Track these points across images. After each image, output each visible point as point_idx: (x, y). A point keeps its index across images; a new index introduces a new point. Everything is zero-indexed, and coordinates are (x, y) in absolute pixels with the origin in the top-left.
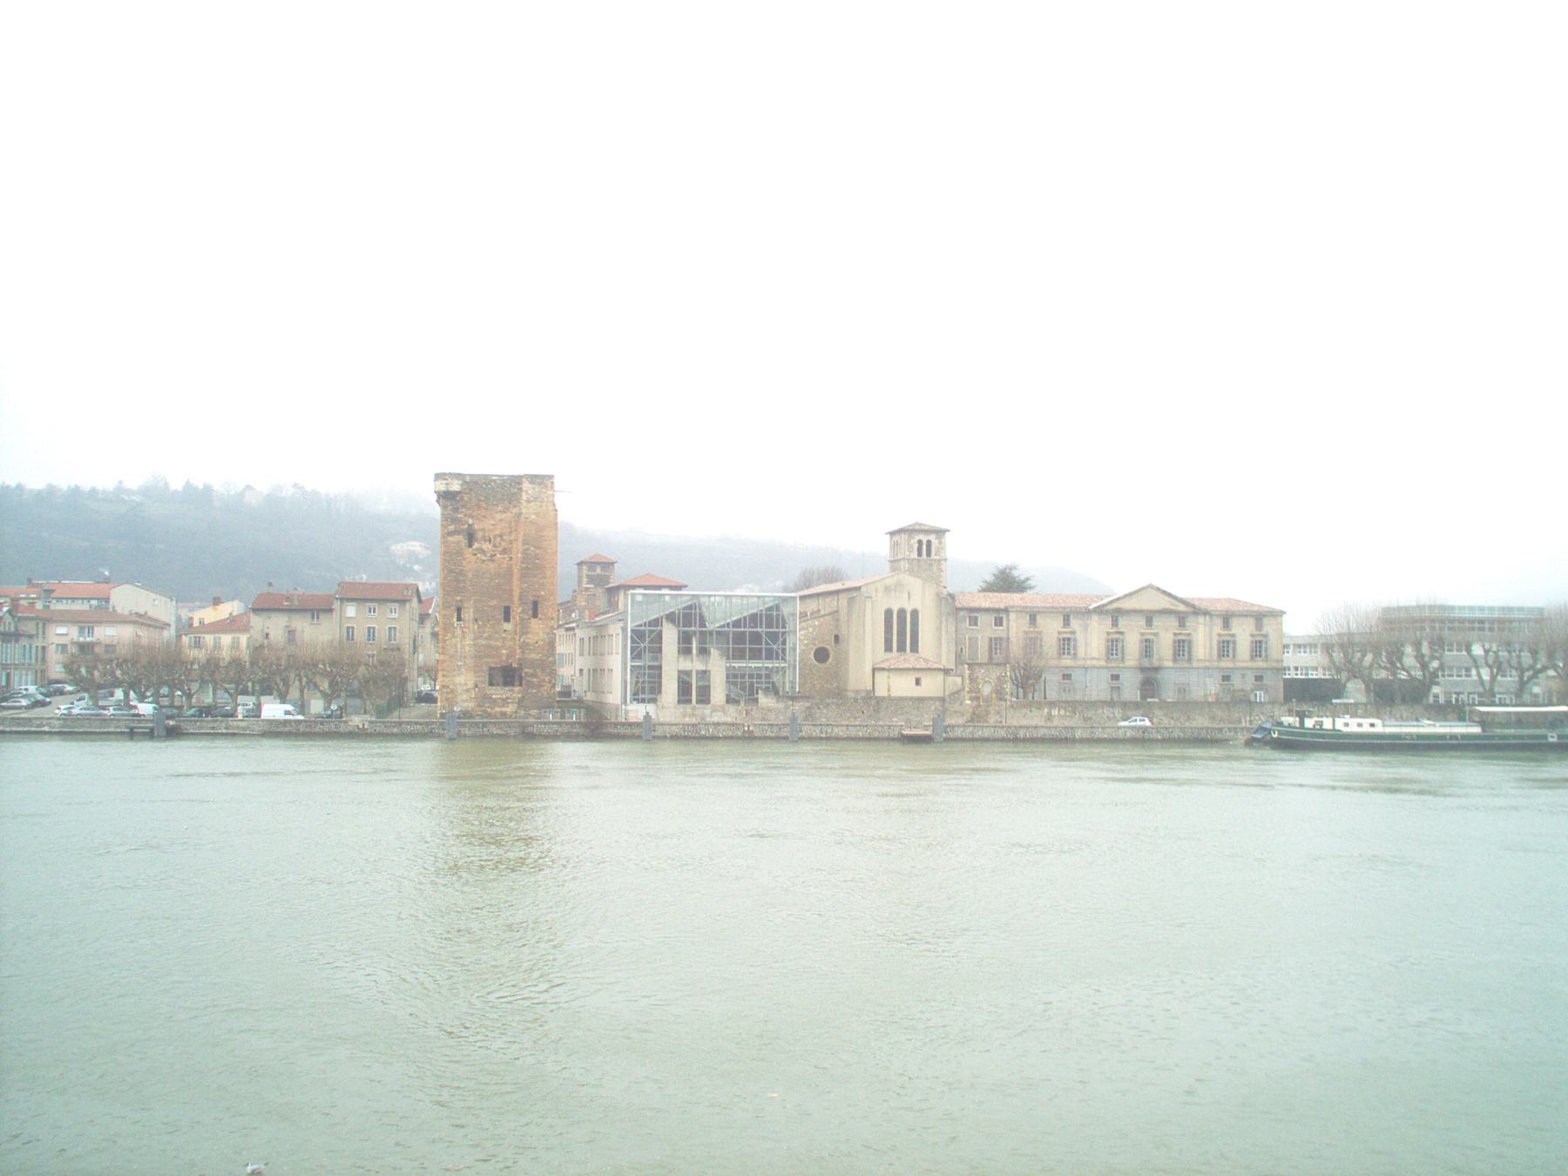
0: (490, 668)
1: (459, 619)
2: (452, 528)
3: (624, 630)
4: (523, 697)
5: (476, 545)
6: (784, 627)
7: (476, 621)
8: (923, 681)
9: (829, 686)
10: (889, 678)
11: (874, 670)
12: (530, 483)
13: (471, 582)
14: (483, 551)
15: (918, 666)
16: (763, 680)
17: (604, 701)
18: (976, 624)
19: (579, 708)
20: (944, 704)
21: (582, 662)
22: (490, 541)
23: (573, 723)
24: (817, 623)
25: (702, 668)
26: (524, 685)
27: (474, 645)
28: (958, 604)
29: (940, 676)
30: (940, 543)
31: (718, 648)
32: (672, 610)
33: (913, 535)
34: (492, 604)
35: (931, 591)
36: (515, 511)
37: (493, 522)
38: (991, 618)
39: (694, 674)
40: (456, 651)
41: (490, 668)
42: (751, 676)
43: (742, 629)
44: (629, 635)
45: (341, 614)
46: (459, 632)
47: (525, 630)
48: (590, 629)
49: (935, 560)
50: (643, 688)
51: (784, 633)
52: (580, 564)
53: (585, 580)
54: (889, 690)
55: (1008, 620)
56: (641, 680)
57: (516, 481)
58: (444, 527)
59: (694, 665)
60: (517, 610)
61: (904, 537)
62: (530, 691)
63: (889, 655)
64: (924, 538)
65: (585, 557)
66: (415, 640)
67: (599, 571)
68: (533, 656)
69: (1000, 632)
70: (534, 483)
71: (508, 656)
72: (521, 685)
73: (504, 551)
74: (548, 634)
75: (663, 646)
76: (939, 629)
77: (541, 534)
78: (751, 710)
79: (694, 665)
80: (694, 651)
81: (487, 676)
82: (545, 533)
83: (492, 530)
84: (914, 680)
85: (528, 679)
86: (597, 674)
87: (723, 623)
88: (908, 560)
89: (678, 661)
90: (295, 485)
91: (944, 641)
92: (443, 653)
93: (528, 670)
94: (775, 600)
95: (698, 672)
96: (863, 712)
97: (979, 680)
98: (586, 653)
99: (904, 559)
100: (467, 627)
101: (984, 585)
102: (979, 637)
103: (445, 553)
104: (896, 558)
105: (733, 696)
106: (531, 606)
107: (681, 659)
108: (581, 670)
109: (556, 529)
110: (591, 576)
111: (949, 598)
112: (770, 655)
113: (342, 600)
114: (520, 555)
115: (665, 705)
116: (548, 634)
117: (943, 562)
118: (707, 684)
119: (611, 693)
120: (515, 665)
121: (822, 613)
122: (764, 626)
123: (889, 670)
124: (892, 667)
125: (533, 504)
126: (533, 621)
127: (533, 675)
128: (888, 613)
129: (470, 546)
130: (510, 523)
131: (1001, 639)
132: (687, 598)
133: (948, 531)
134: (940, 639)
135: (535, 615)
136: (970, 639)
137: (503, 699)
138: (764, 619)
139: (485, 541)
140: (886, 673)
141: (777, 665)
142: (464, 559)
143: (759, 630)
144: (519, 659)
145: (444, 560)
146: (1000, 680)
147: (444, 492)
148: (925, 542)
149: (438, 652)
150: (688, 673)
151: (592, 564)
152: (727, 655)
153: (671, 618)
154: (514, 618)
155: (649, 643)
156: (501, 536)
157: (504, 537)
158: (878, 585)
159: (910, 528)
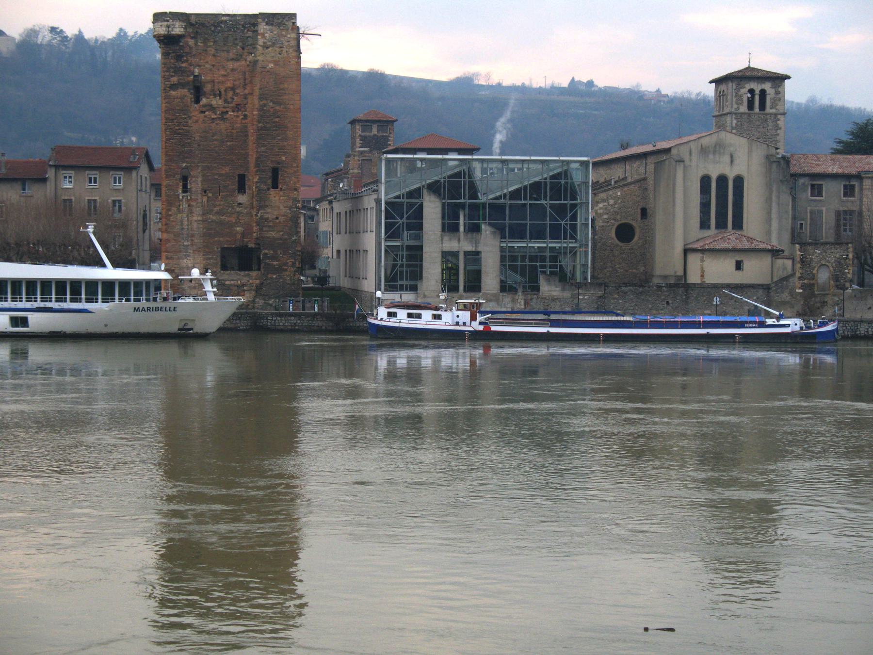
0: (223, 249)
1: (185, 190)
2: (175, 79)
3: (378, 201)
4: (262, 284)
5: (204, 101)
6: (574, 198)
7: (205, 192)
8: (746, 265)
9: (634, 271)
10: (702, 261)
11: (686, 251)
12: (267, 24)
13: (199, 145)
14: (212, 108)
15: (740, 246)
16: (548, 264)
17: (359, 289)
18: (820, 194)
19: (322, 296)
20: (769, 292)
21: (339, 242)
22: (220, 95)
23: (316, 315)
24: (619, 194)
25: (469, 248)
26: (262, 270)
27: (203, 221)
28: (794, 169)
29: (767, 259)
30: (777, 93)
31: (490, 224)
32: (436, 178)
33: (742, 83)
34: (223, 172)
35: (759, 153)
36: (250, 58)
37: (223, 73)
38: (837, 187)
39: (461, 257)
40: (183, 229)
41: (223, 249)
42: (533, 259)
43: (563, 202)
44: (383, 208)
45: (56, 184)
46: (185, 205)
47: (262, 202)
48: (346, 202)
49: (771, 114)
50: (401, 273)
51: (574, 206)
52: (353, 122)
53: (358, 142)
54: (702, 276)
55: (861, 189)
56: (400, 263)
57: (250, 22)
58: (165, 78)
59: (462, 244)
60: (253, 179)
61: (731, 86)
62: (269, 276)
63: (706, 233)
64: (757, 87)
65: (360, 115)
66: (145, 216)
67: (375, 131)
68: (273, 234)
69: (851, 203)
70: (272, 25)
71: (243, 235)
72: (259, 270)
73: (237, 108)
74: (290, 208)
75: (425, 222)
76: (769, 200)
77: (282, 86)
78: (531, 299)
79: (462, 244)
80: (462, 228)
81: (219, 259)
82: (286, 86)
83: (223, 83)
84: (734, 263)
85: (267, 261)
86: (354, 254)
87: (498, 194)
88: (735, 114)
89: (442, 240)
90: (53, 30)
91: (774, 215)
92: (166, 231)
93: (266, 251)
94: (562, 166)
95: (466, 254)
96: (668, 303)
97: (813, 264)
98: (343, 230)
99: (730, 113)
100: (196, 200)
101: (839, 147)
102: (824, 209)
103: (167, 111)
104: (721, 113)
105: (510, 282)
106: (270, 174)
107: (446, 238)
108: (339, 252)
109: (299, 80)
110: (365, 137)
111: (782, 162)
112: (556, 233)
113: (57, 167)
114: (255, 113)
115: (426, 293)
116: (290, 208)
117: (781, 118)
118: (476, 268)
119: (366, 279)
120: (251, 245)
121: (629, 180)
122: (548, 198)
123: (703, 251)
124: (707, 247)
125: (270, 49)
126: (272, 192)
127: (274, 258)
128: (705, 181)
129: (197, 101)
130: (245, 73)
131: (851, 212)
132: (456, 163)
133: (788, 77)
134: (769, 213)
135: (275, 185)
136: (812, 212)
137: (238, 286)
138: (447, 184)
139: (215, 96)
140: (699, 255)
141: (565, 245)
142: (190, 117)
143: (543, 202)
144: (257, 239)
145: (167, 119)
146: (840, 264)
147: (164, 36)
148: (757, 92)
149: (160, 230)
150: (455, 254)
151: (366, 123)
152: (500, 231)
153: (434, 188)
154: (250, 189)
155: (408, 218)
156: (233, 89)
157: (237, 91)
158: (693, 146)
159: (740, 74)
